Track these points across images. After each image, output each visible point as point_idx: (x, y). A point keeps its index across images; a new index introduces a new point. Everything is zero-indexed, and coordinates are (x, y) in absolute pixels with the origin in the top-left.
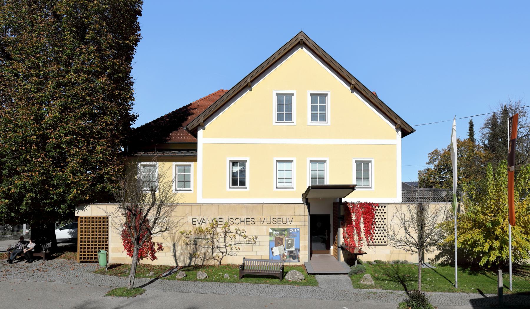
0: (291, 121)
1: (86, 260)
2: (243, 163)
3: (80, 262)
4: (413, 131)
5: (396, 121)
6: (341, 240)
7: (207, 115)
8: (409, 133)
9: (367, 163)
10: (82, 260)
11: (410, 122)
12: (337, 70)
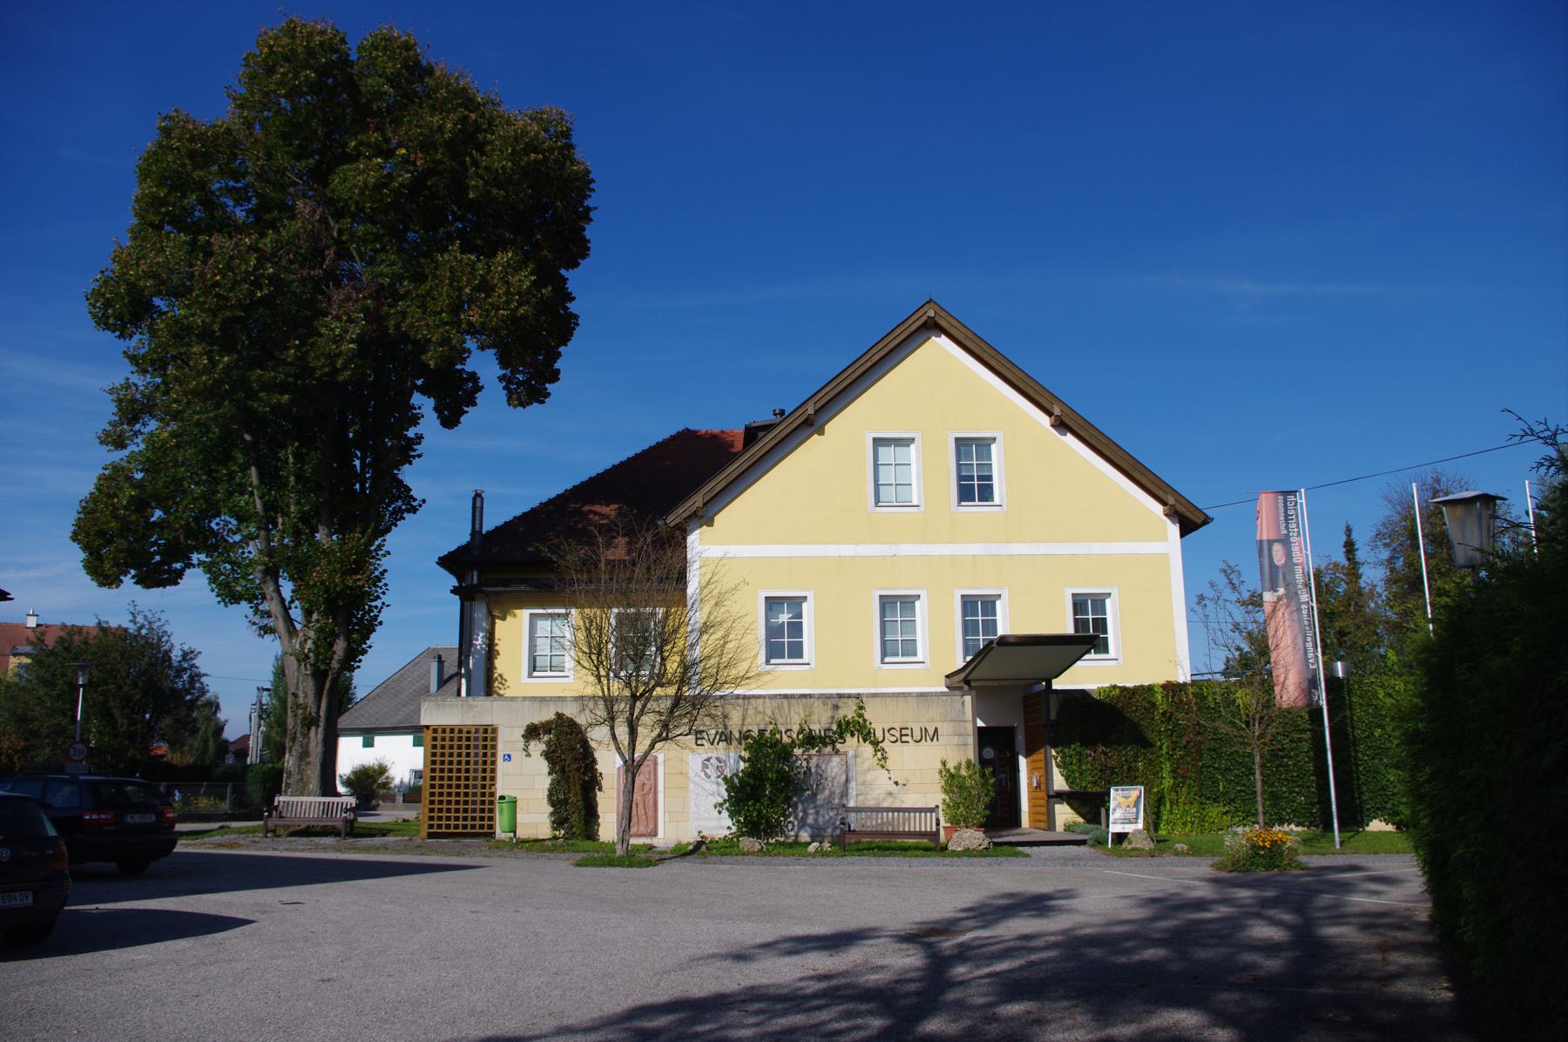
0: (993, 501)
1: (477, 830)
2: (796, 603)
3: (426, 836)
4: (1207, 521)
5: (1165, 499)
6: (1055, 778)
7: (1157, 486)
8: (1196, 527)
9: (908, 602)
10: (435, 830)
11: (1200, 499)
12: (1017, 383)
